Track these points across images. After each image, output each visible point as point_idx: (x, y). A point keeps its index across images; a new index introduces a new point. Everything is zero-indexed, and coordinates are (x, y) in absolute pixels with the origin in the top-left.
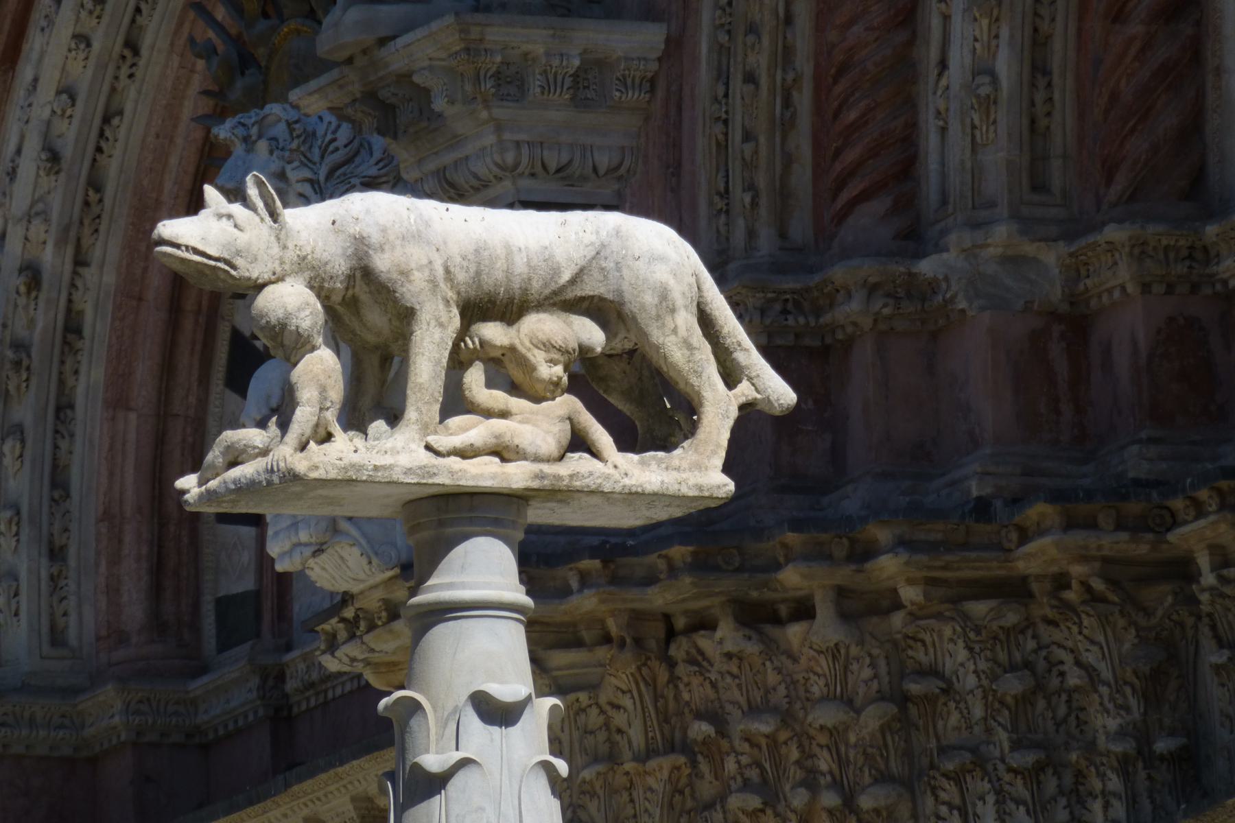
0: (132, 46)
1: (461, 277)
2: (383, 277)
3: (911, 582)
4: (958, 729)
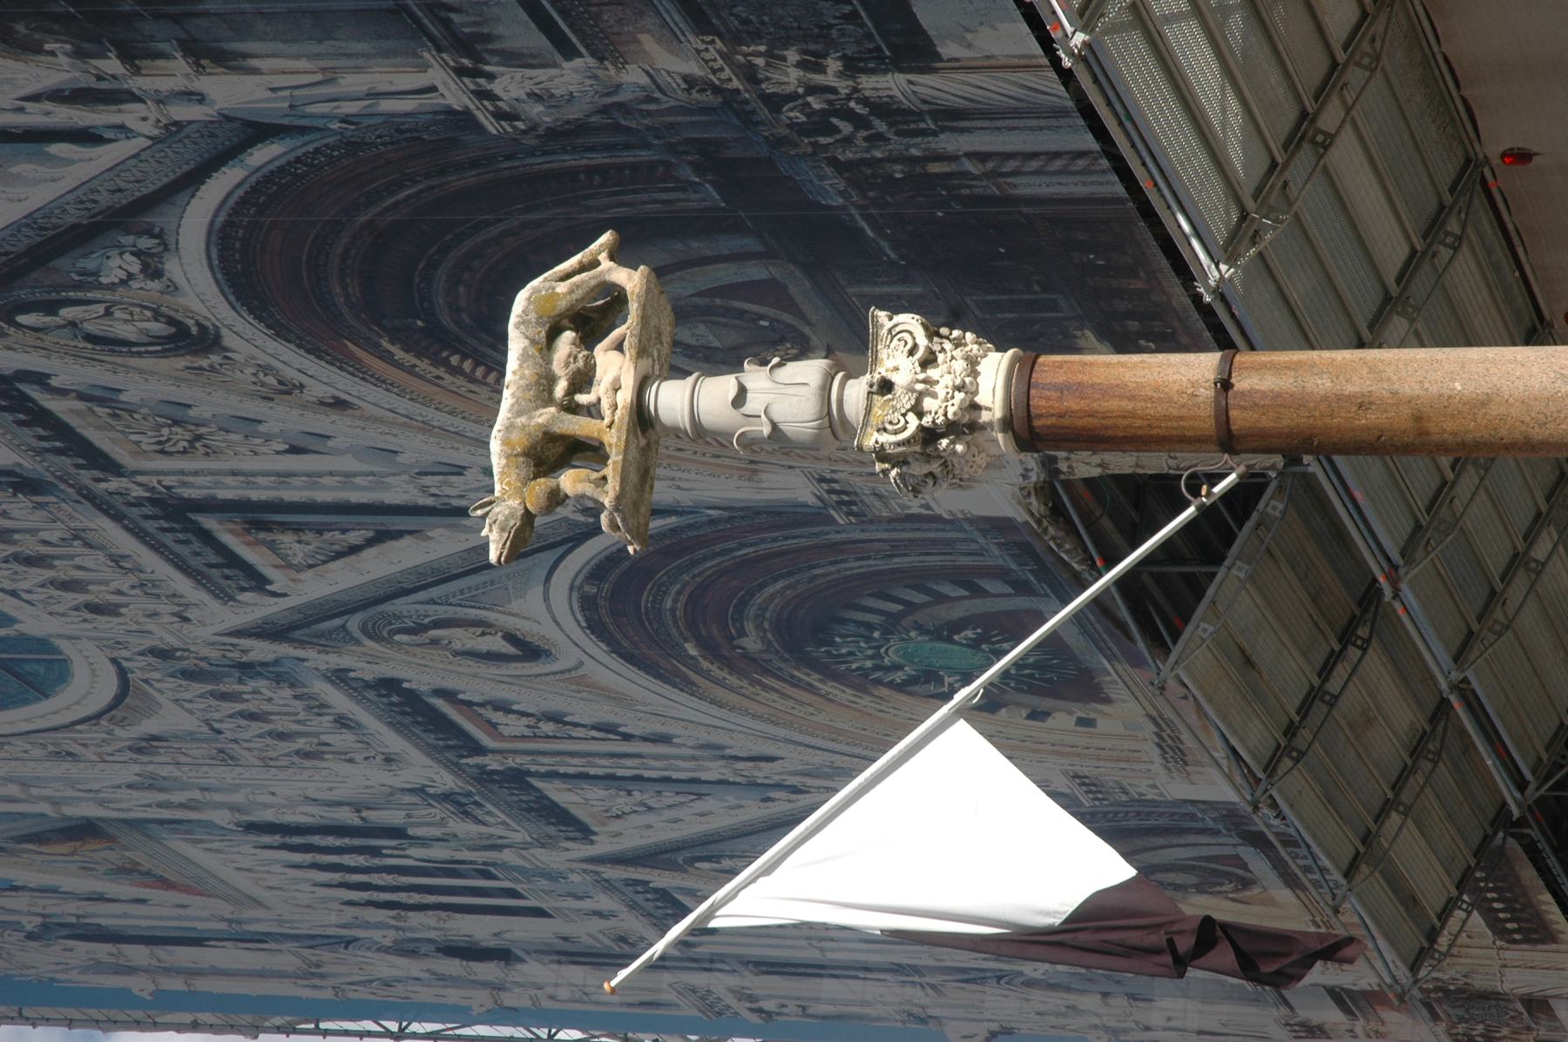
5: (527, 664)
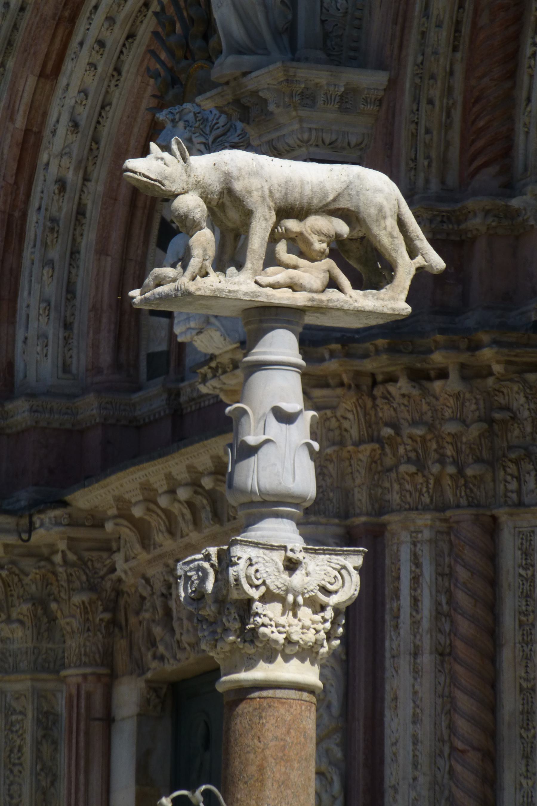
0: (118, 70)
1: (277, 195)
2: (238, 193)
3: (498, 362)
4: (518, 437)
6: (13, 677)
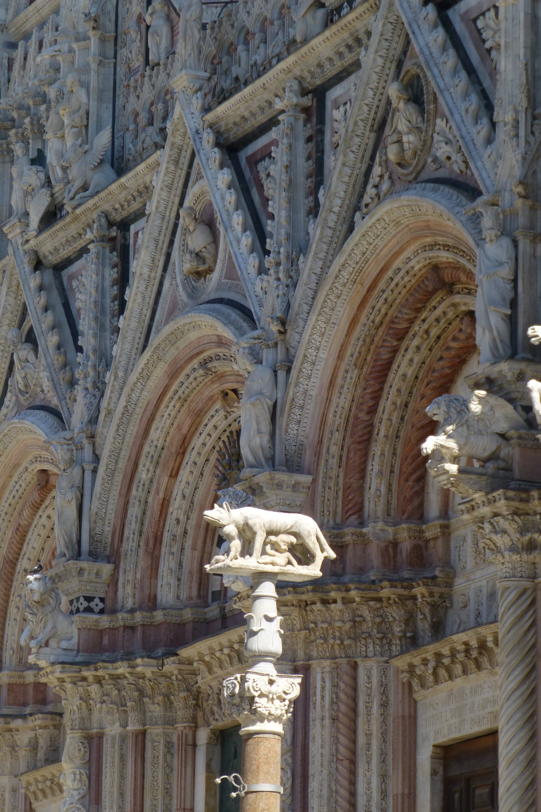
0: (202, 474)
5: (103, 793)
6: (155, 727)
